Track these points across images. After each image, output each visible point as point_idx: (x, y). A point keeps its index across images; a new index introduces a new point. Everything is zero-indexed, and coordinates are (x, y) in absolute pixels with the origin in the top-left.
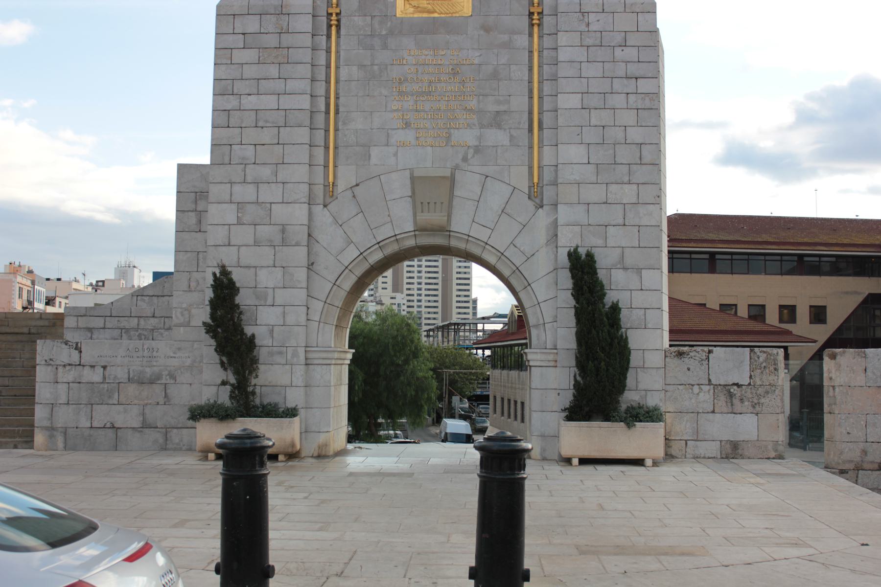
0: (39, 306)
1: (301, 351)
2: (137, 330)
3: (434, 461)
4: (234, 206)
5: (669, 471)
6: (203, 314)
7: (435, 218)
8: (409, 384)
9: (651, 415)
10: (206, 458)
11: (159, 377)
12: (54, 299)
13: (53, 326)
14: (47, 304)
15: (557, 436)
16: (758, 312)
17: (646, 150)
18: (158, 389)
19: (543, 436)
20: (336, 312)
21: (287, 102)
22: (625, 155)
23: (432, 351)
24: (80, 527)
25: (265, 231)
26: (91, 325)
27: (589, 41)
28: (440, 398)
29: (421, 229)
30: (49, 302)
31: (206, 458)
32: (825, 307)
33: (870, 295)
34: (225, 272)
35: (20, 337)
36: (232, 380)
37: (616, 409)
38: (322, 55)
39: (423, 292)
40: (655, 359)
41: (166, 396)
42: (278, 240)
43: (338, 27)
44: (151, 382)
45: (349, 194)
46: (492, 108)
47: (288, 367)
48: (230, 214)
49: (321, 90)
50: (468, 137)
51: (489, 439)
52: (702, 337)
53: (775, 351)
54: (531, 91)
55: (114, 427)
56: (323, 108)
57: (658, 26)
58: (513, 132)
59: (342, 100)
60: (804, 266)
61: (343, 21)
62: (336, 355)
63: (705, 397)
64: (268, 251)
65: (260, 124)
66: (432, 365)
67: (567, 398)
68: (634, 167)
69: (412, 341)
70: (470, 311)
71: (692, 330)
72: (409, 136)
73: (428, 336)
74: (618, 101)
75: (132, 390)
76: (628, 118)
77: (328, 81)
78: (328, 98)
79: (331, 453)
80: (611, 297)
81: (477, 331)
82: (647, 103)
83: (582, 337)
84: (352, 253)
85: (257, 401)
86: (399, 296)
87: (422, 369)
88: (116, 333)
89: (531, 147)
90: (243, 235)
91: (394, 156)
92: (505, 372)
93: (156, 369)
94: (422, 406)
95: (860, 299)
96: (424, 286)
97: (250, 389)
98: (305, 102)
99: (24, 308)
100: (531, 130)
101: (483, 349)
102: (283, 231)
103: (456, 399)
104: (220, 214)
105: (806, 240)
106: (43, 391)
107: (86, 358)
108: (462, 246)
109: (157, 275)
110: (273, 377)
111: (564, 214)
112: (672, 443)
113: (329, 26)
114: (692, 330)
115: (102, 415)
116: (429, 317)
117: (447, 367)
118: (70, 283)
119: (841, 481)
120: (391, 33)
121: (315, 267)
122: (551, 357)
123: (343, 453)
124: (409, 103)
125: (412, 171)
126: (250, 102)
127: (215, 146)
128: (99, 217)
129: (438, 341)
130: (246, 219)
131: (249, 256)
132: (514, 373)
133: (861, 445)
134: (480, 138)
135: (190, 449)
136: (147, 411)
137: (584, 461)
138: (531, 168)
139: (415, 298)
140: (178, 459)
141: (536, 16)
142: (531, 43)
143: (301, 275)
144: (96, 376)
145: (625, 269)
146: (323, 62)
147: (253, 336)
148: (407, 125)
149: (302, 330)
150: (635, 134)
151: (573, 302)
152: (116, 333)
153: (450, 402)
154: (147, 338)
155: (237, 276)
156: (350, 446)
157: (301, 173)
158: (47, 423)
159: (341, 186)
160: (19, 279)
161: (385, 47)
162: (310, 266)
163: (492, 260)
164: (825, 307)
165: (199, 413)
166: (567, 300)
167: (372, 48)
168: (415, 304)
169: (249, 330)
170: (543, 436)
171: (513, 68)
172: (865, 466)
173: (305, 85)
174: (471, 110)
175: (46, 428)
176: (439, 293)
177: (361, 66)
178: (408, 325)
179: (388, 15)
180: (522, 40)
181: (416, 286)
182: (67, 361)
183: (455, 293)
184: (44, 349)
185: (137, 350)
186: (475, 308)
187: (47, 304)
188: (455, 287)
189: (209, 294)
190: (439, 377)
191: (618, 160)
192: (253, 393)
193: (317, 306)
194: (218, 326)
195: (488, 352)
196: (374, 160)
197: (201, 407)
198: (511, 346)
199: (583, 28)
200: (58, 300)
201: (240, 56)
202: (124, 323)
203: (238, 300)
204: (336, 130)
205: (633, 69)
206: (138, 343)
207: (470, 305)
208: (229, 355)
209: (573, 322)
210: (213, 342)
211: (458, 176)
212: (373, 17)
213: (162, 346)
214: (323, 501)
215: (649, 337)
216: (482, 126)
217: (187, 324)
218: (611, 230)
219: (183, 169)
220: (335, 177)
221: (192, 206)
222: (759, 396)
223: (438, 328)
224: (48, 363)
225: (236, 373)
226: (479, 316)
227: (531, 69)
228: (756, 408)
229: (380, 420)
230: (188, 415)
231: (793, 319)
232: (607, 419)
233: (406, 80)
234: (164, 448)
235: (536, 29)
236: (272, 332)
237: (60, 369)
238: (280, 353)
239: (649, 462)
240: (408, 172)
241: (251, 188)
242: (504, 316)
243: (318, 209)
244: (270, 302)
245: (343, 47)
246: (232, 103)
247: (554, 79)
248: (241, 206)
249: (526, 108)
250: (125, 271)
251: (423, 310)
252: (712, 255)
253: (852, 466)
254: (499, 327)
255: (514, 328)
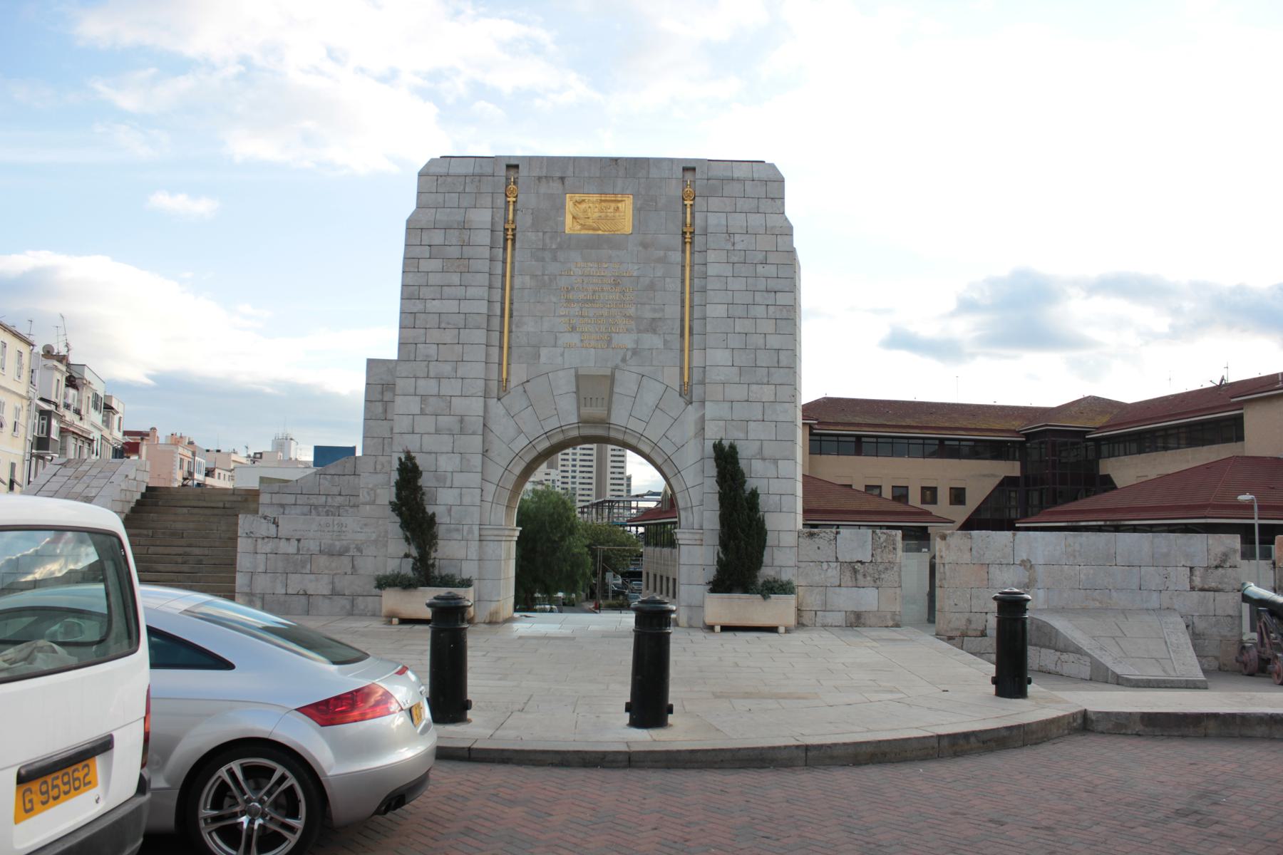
0: (199, 477)
1: (476, 528)
2: (324, 506)
3: (592, 628)
4: (418, 399)
5: (799, 637)
6: (388, 494)
7: (597, 411)
8: (565, 560)
9: (784, 588)
10: (390, 623)
11: (347, 550)
12: (213, 470)
13: (246, 500)
14: (207, 475)
15: (702, 607)
16: (901, 494)
17: (783, 355)
18: (346, 560)
19: (689, 606)
20: (507, 494)
21: (467, 307)
22: (764, 358)
23: (587, 528)
24: (358, 655)
25: (444, 421)
26: (284, 502)
27: (735, 259)
28: (595, 574)
29: (584, 422)
30: (209, 473)
31: (390, 623)
32: (964, 489)
33: (1006, 478)
34: (409, 457)
35: (216, 511)
36: (414, 552)
37: (754, 583)
38: (499, 265)
39: (578, 469)
40: (789, 539)
41: (353, 567)
42: (457, 428)
43: (514, 240)
44: (340, 555)
45: (520, 388)
46: (648, 314)
47: (463, 543)
48: (414, 405)
49: (497, 296)
50: (627, 340)
51: (642, 602)
52: (848, 517)
53: (894, 532)
54: (683, 301)
55: (306, 594)
56: (498, 312)
57: (795, 245)
58: (668, 338)
59: (515, 306)
60: (945, 450)
61: (518, 236)
62: (507, 533)
63: (833, 573)
64: (447, 439)
65: (443, 325)
66: (587, 542)
67: (711, 573)
68: (772, 370)
69: (568, 519)
70: (624, 487)
71: (824, 512)
72: (574, 339)
73: (582, 513)
74: (759, 311)
75: (323, 561)
76: (768, 326)
77: (503, 289)
78: (503, 303)
79: (501, 619)
80: (751, 484)
81: (631, 508)
82: (785, 315)
83: (725, 519)
84: (522, 442)
85: (436, 573)
86: (553, 471)
87: (578, 545)
88: (306, 509)
89: (682, 350)
90: (426, 424)
91: (563, 355)
92: (658, 549)
93: (345, 543)
94: (577, 582)
95: (997, 481)
96: (578, 463)
97: (431, 562)
98: (482, 307)
99: (185, 479)
100: (682, 335)
101: (637, 526)
102: (461, 421)
103: (609, 576)
104: (405, 405)
105: (947, 425)
106: (243, 561)
107: (283, 532)
108: (620, 437)
109: (324, 455)
110: (452, 551)
111: (710, 410)
112: (804, 614)
113: (506, 240)
114: (824, 512)
115: (296, 583)
116: (583, 495)
117: (601, 544)
118: (229, 454)
119: (945, 645)
120: (560, 247)
121: (489, 454)
122: (697, 537)
123: (510, 620)
124: (575, 309)
125: (576, 369)
126: (435, 306)
127: (402, 344)
128: (268, 390)
129: (592, 518)
130: (429, 410)
131: (430, 442)
132: (666, 550)
133: (967, 615)
134: (637, 342)
135: (374, 615)
136: (336, 580)
137: (725, 629)
138: (682, 368)
139: (570, 474)
140: (366, 623)
141: (688, 235)
142: (684, 258)
143: (477, 460)
144: (291, 548)
145: (764, 459)
146: (499, 271)
147: (434, 514)
148: (573, 329)
149: (476, 509)
150: (774, 342)
151: (717, 488)
152: (306, 509)
153: (604, 578)
154: (333, 515)
155: (420, 461)
156: (517, 615)
157: (478, 370)
158: (247, 590)
159: (514, 382)
160: (180, 450)
161: (555, 259)
162: (485, 453)
163: (647, 450)
164: (964, 489)
165: (384, 583)
166: (712, 486)
167: (543, 260)
168: (570, 480)
169: (430, 510)
170: (689, 606)
171: (668, 280)
172: (970, 633)
173: (483, 292)
174: (630, 317)
175: (246, 594)
176: (594, 470)
177: (533, 276)
178: (564, 503)
179: (558, 232)
180: (676, 256)
181: (570, 463)
182: (265, 534)
183: (609, 470)
184: (245, 523)
185: (327, 525)
186: (629, 485)
187: (207, 475)
188: (609, 464)
189: (395, 476)
190: (593, 554)
191: (759, 364)
192: (433, 565)
193: (490, 488)
194: (402, 505)
195: (641, 530)
196: (543, 359)
197: (386, 577)
198: (665, 524)
199: (729, 247)
200: (217, 471)
201: (425, 265)
202: (314, 500)
203: (420, 482)
204: (510, 331)
205: (772, 284)
206: (324, 519)
207: (624, 482)
208: (412, 531)
209: (717, 506)
210: (398, 519)
211: (618, 374)
212: (544, 233)
213: (350, 522)
214: (499, 658)
215: (785, 518)
216: (639, 331)
217: (373, 503)
218: (752, 424)
219: (372, 364)
220: (508, 373)
221: (379, 397)
222: (879, 572)
223: (592, 505)
224: (249, 535)
225: (419, 547)
226: (633, 493)
227: (683, 281)
228: (877, 583)
229: (537, 595)
230: (375, 583)
231: (934, 501)
232: (746, 591)
233: (573, 289)
234: (351, 613)
235: (688, 246)
236: (450, 511)
237: (260, 541)
238: (458, 530)
239: (782, 629)
240: (573, 371)
241: (433, 383)
242: (658, 494)
243: (493, 402)
244: (448, 484)
245: (517, 258)
246: (418, 306)
247: (704, 290)
248: (424, 398)
249: (679, 289)
250: (282, 443)
251: (577, 486)
252: (859, 437)
253: (958, 633)
254: (652, 505)
255: (667, 507)
